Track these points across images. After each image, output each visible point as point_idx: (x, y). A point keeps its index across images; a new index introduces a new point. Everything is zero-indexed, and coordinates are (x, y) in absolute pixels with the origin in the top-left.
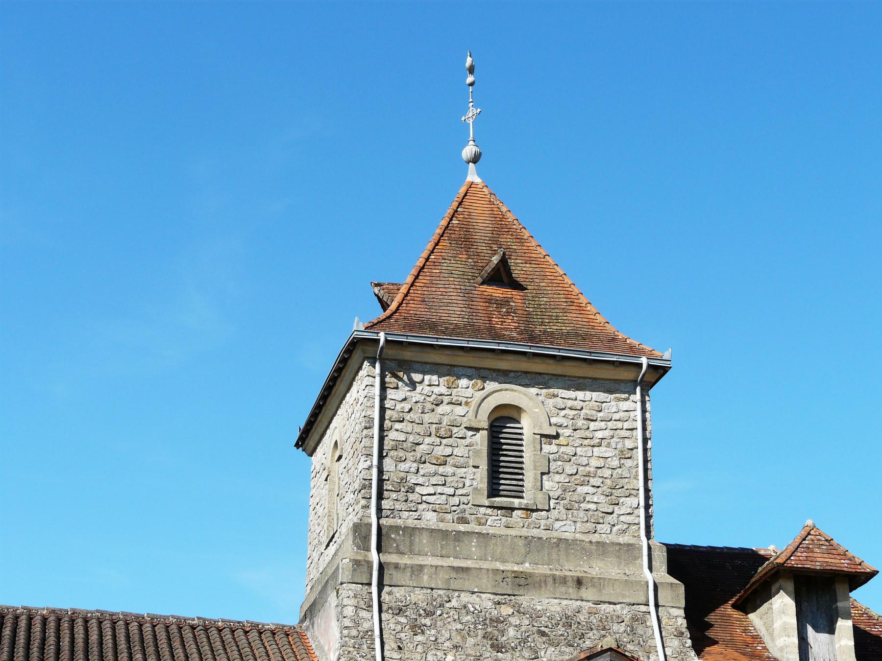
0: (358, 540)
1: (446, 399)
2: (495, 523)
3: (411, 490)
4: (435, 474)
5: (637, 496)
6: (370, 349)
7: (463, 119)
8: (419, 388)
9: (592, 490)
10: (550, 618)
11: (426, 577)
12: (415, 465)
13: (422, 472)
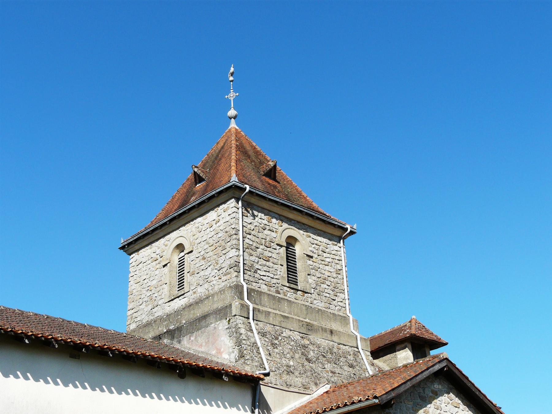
0: (238, 294)
1: (268, 228)
2: (290, 295)
3: (255, 272)
4: (265, 266)
5: (344, 293)
6: (237, 193)
7: (226, 97)
8: (257, 219)
9: (327, 287)
10: (324, 348)
11: (271, 319)
12: (257, 259)
13: (260, 263)
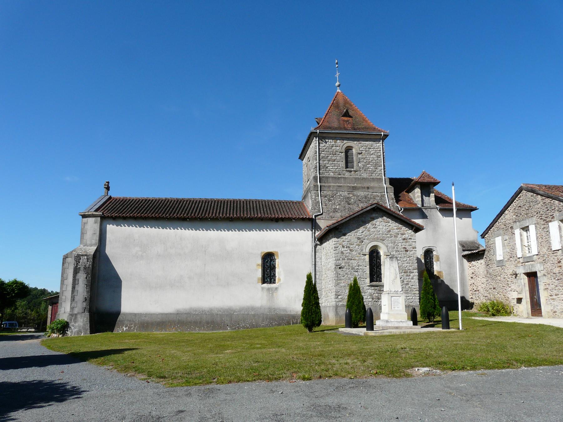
2: (347, 175)
3: (327, 168)
